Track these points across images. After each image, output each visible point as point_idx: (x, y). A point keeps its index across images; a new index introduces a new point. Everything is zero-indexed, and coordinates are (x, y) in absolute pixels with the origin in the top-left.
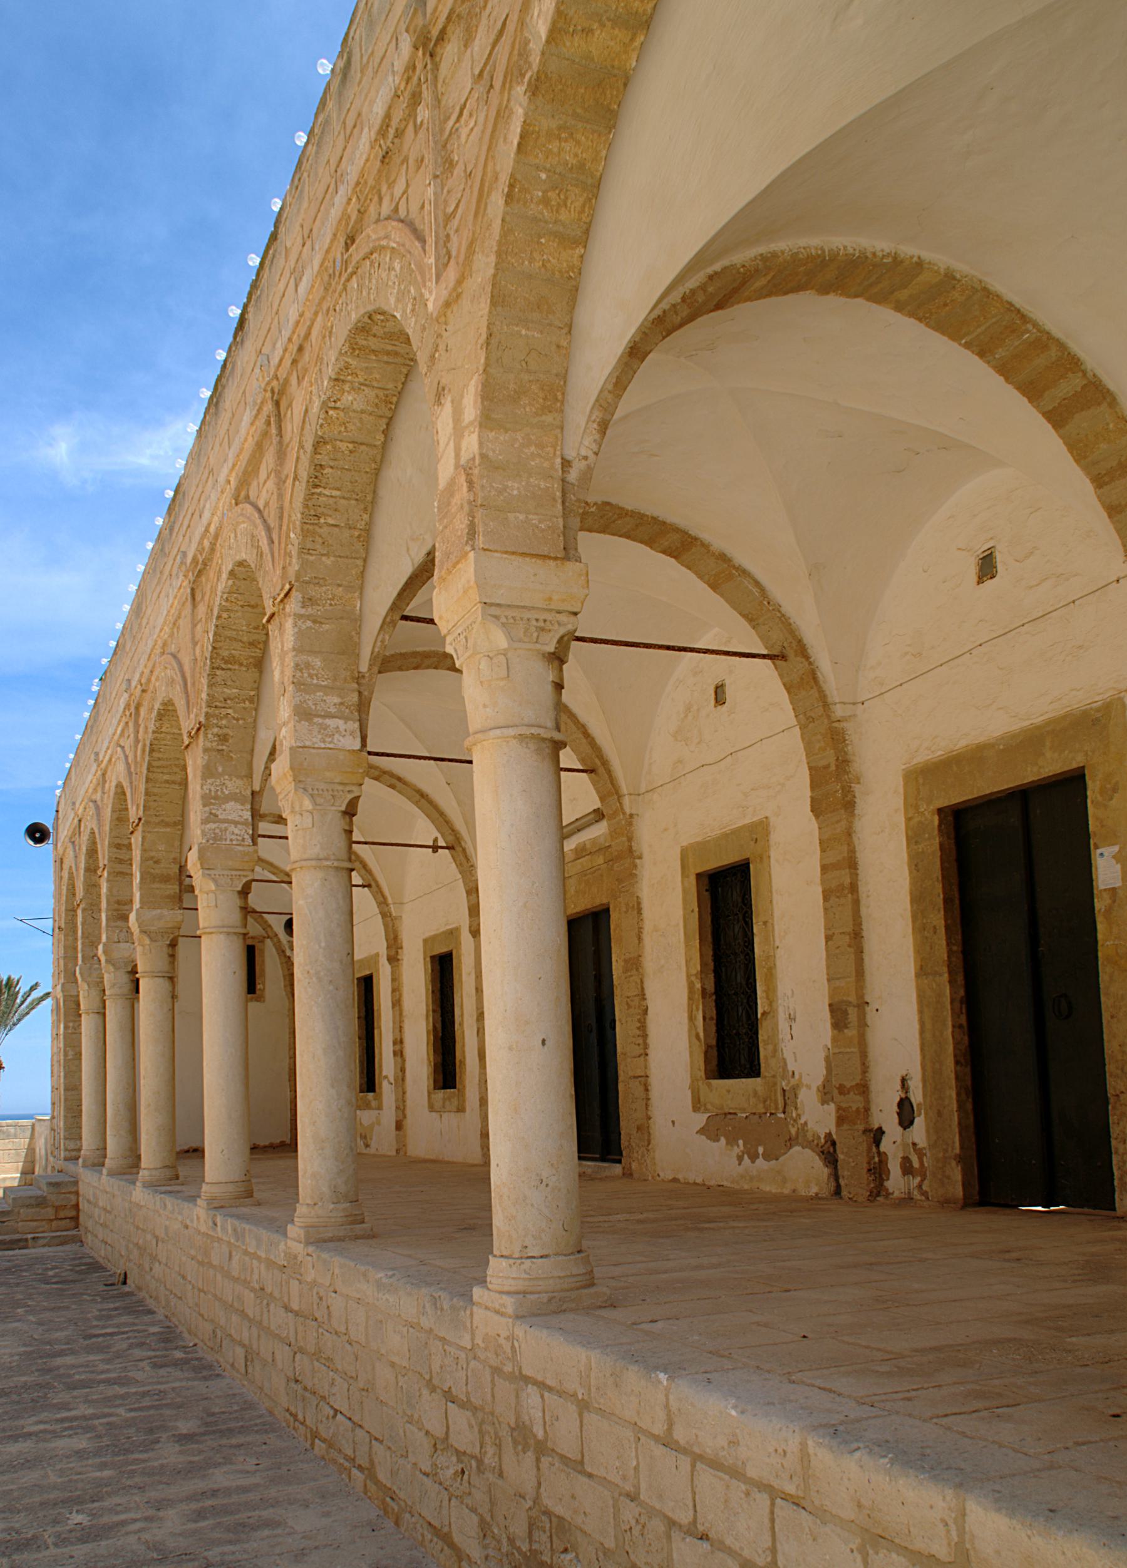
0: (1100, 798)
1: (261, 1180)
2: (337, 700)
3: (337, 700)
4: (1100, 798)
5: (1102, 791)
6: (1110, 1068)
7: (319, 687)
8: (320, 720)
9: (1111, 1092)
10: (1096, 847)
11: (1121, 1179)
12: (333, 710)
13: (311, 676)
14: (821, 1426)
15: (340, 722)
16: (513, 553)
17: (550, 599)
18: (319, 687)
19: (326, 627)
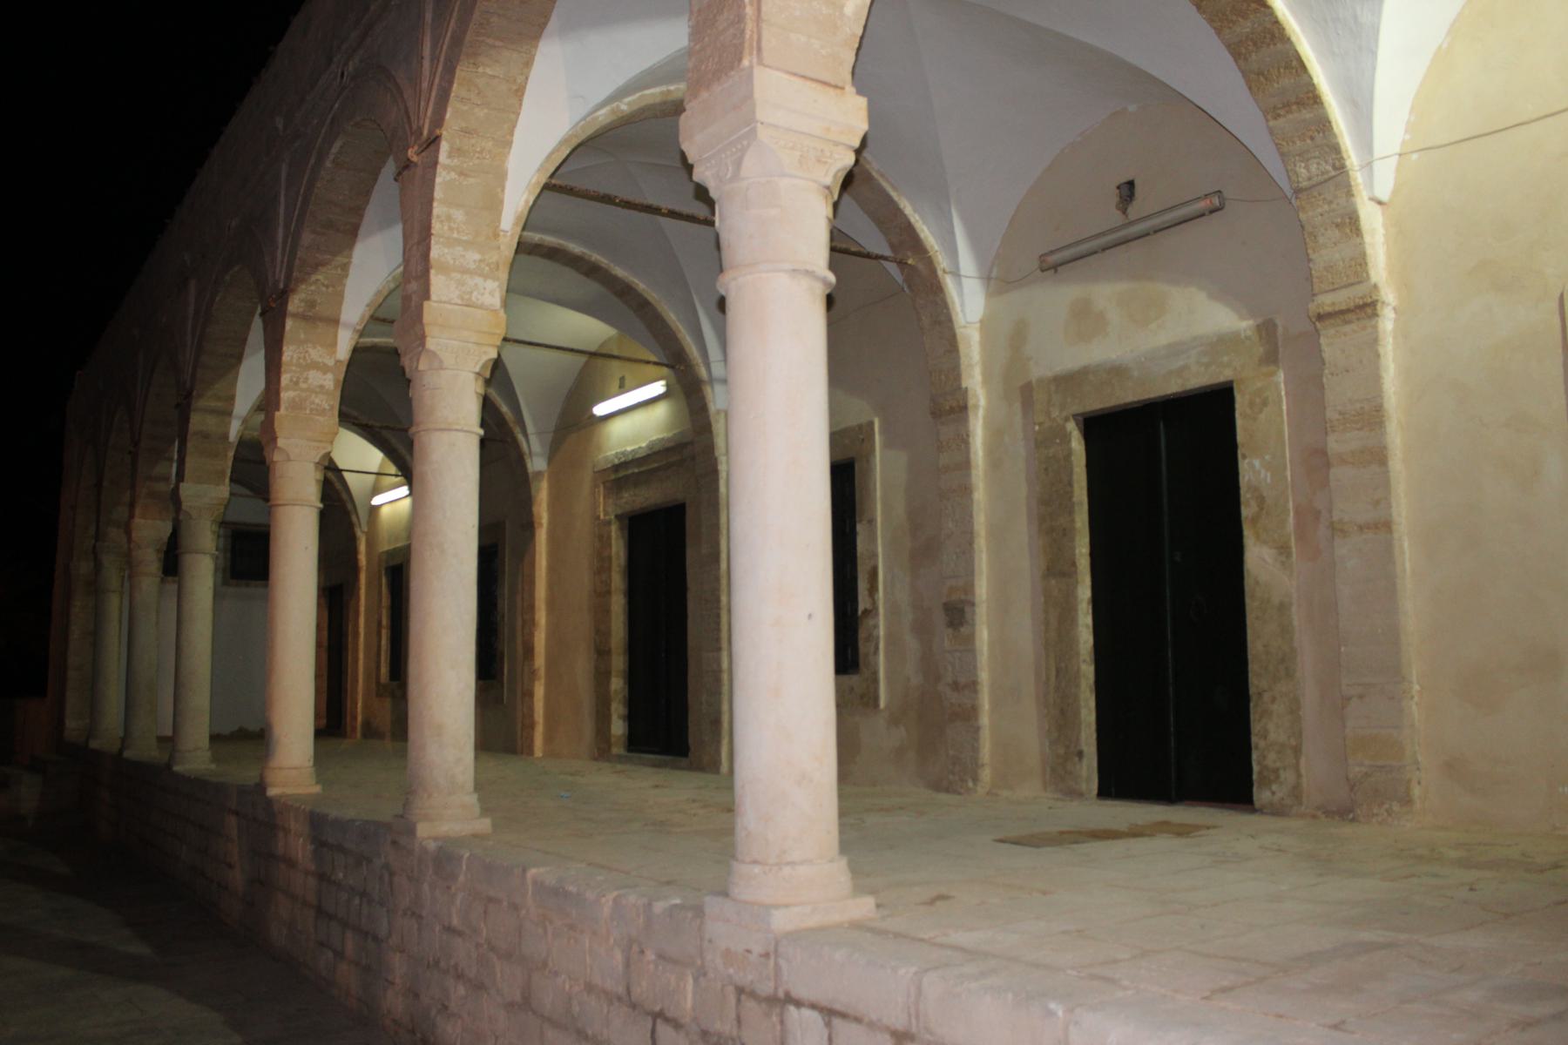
0: (1248, 411)
1: (1053, 679)
2: (477, 257)
3: (477, 257)
4: (1248, 411)
5: (1252, 404)
6: (1253, 667)
7: (458, 242)
8: (458, 276)
9: (1252, 690)
10: (1244, 457)
11: (1260, 773)
12: (472, 266)
13: (451, 229)
14: (1214, 992)
15: (479, 280)
16: (795, 74)
17: (828, 130)
18: (458, 242)
19: (471, 180)
